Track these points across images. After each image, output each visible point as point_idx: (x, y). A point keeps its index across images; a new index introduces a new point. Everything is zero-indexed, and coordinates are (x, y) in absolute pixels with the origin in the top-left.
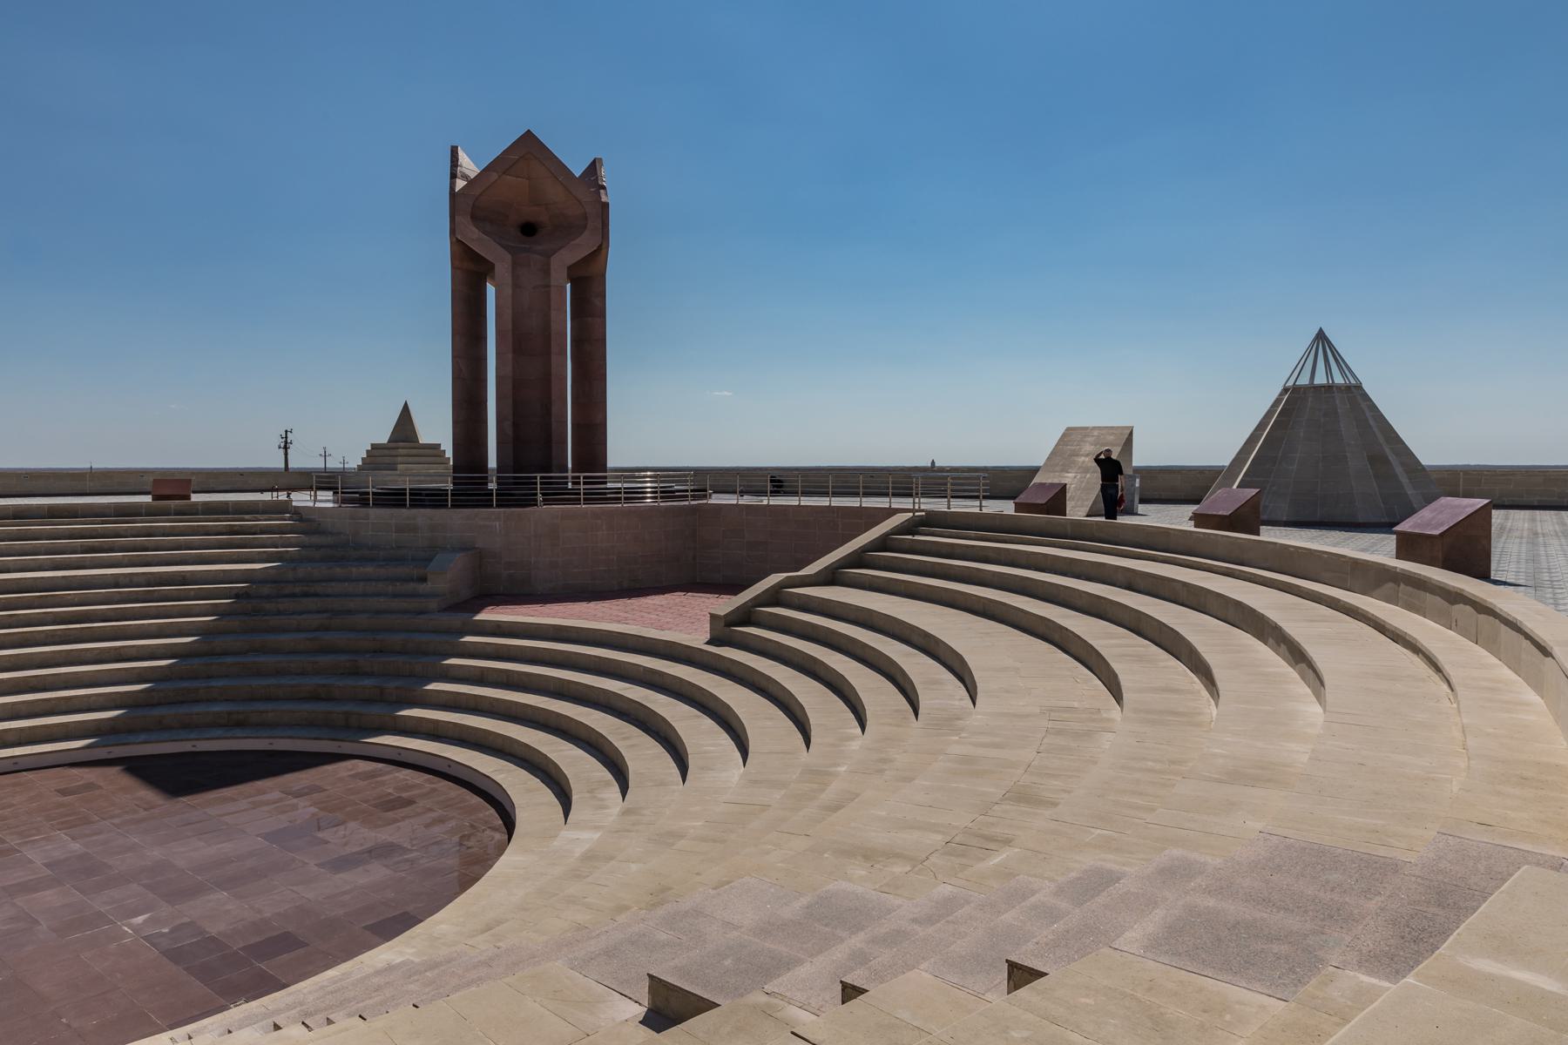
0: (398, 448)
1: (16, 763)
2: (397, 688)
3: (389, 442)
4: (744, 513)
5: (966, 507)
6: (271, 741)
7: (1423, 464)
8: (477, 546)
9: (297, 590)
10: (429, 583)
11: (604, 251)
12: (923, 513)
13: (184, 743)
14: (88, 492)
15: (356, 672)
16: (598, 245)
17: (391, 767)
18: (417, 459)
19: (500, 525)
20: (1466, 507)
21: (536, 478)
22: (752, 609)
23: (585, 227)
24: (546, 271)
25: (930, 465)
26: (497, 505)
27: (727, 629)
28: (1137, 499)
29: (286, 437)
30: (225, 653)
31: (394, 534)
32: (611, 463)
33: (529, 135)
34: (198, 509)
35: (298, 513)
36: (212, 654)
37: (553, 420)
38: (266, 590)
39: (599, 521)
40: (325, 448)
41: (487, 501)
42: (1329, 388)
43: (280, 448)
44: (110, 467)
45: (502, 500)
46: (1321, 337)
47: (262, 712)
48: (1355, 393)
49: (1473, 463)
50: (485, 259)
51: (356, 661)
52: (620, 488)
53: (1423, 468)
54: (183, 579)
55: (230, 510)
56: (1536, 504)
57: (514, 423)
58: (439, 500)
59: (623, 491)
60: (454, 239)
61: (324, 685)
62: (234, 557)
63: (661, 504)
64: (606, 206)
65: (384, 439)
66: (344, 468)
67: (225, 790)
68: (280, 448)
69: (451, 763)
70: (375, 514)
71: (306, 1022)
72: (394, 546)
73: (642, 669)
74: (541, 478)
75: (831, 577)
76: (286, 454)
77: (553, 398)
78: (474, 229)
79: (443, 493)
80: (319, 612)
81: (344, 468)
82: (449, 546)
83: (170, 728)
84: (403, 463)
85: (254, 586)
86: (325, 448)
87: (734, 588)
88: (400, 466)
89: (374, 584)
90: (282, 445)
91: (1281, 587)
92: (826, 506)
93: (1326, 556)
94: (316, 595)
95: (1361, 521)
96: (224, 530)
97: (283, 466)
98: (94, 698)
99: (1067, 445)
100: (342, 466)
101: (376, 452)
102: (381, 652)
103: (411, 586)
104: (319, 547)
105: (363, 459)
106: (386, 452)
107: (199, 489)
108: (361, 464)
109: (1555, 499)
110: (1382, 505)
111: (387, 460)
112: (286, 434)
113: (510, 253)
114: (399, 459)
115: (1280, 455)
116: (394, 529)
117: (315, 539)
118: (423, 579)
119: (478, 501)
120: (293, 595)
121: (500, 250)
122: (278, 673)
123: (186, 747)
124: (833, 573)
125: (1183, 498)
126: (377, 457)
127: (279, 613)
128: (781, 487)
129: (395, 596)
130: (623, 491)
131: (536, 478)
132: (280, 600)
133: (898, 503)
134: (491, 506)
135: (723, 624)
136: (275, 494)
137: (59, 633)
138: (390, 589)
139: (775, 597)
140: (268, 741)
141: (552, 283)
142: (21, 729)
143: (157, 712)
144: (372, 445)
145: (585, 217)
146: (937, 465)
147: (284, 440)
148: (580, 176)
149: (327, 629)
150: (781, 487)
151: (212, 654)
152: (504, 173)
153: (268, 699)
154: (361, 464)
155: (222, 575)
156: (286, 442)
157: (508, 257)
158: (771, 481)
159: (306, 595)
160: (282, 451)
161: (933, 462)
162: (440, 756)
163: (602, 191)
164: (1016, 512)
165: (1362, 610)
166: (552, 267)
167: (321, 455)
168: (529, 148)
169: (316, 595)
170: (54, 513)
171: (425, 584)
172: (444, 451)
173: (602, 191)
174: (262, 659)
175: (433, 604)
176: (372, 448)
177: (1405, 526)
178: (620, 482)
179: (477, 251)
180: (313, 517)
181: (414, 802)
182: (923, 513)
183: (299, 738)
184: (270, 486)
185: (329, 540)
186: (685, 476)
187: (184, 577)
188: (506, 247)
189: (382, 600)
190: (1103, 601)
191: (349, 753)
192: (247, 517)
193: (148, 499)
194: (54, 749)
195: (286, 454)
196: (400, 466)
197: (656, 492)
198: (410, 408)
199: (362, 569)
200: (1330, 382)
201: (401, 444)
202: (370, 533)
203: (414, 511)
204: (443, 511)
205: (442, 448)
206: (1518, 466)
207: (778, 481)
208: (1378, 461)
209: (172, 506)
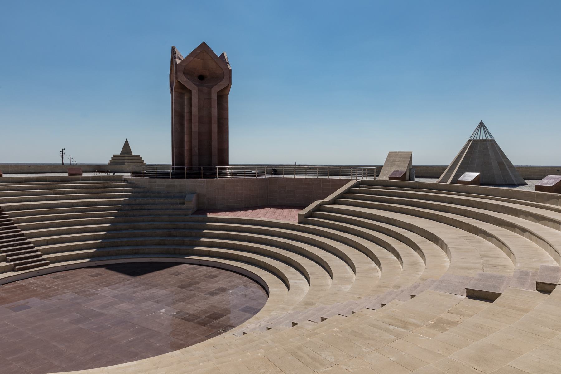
5: (372, 179)
7: (514, 165)
11: (229, 86)
12: (360, 181)
14: (9, 172)
17: (199, 266)
20: (558, 178)
21: (201, 168)
22: (313, 212)
23: (224, 77)
24: (209, 94)
25: (294, 164)
26: (203, 178)
27: (305, 219)
28: (414, 177)
29: (63, 152)
30: (121, 230)
34: (90, 179)
35: (126, 180)
36: (115, 230)
38: (127, 208)
40: (70, 156)
42: (485, 140)
43: (60, 155)
44: (27, 163)
45: (205, 176)
48: (492, 141)
49: (422, 165)
50: (186, 87)
51: (170, 232)
52: (244, 172)
53: (514, 167)
54: (96, 204)
55: (101, 179)
56: (536, 178)
60: (177, 81)
61: (162, 240)
62: (109, 196)
64: (230, 70)
65: (119, 153)
67: (149, 274)
68: (60, 155)
69: (221, 264)
70: (159, 181)
71: (234, 334)
74: (203, 168)
75: (334, 202)
76: (63, 158)
77: (212, 139)
79: (168, 173)
85: (123, 206)
86: (70, 156)
87: (302, 207)
88: (126, 163)
90: (61, 155)
91: (510, 202)
92: (316, 178)
93: (525, 192)
95: (497, 183)
97: (62, 163)
98: (83, 245)
99: (391, 158)
100: (73, 163)
101: (116, 158)
102: (176, 228)
105: (110, 160)
106: (120, 158)
107: (51, 172)
108: (109, 162)
110: (503, 179)
111: (120, 161)
112: (62, 150)
114: (126, 161)
115: (470, 162)
116: (166, 186)
117: (136, 190)
118: (184, 204)
120: (137, 209)
121: (193, 85)
123: (121, 261)
124: (335, 200)
125: (421, 176)
128: (276, 171)
129: (174, 209)
133: (353, 178)
134: (201, 178)
135: (304, 217)
136: (96, 173)
137: (61, 223)
138: (172, 207)
139: (319, 208)
140: (150, 259)
141: (212, 98)
142: (64, 256)
143: (107, 250)
145: (223, 74)
146: (297, 164)
147: (62, 152)
149: (153, 221)
150: (276, 171)
151: (115, 230)
154: (109, 162)
155: (109, 202)
156: (62, 154)
157: (197, 88)
158: (273, 169)
159: (141, 209)
160: (61, 157)
161: (295, 163)
162: (217, 262)
165: (523, 210)
167: (68, 159)
168: (203, 48)
169: (145, 209)
170: (38, 180)
172: (141, 158)
175: (190, 212)
180: (133, 182)
181: (218, 276)
182: (360, 181)
187: (96, 203)
188: (196, 85)
190: (447, 207)
192: (108, 182)
193: (66, 175)
194: (66, 264)
195: (63, 158)
196: (126, 163)
197: (231, 174)
200: (487, 138)
201: (126, 155)
202: (157, 187)
207: (275, 169)
208: (501, 164)
209: (80, 178)
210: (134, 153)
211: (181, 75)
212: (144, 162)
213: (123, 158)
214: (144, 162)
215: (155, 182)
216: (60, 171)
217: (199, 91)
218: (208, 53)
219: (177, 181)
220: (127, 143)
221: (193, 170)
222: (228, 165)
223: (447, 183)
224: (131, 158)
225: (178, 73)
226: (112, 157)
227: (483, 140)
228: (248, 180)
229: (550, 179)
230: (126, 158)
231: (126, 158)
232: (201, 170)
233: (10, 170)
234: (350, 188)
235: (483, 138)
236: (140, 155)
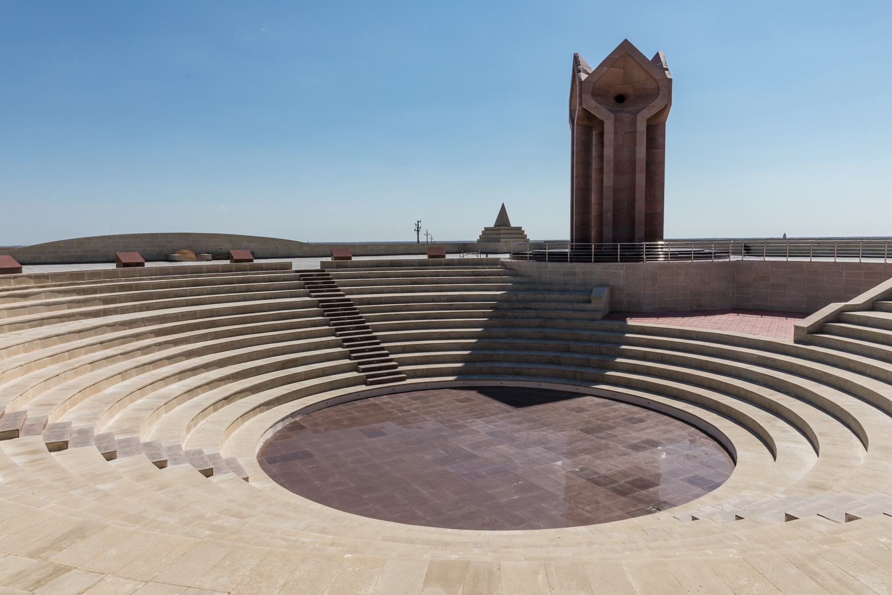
1: (614, 395)
2: (598, 360)
3: (495, 226)
4: (770, 266)
6: (577, 387)
8: (610, 284)
9: (521, 306)
10: (592, 304)
11: (667, 109)
13: (567, 386)
15: (568, 350)
16: (665, 105)
17: (612, 402)
18: (510, 236)
19: (623, 272)
21: (617, 245)
23: (658, 94)
25: (782, 237)
26: (620, 261)
27: (809, 336)
30: (496, 337)
31: (562, 277)
34: (455, 263)
37: (636, 211)
39: (680, 271)
40: (427, 231)
41: (543, 258)
43: (415, 230)
45: (598, 258)
47: (529, 368)
55: (470, 263)
57: (613, 214)
58: (587, 258)
59: (693, 252)
61: (556, 357)
63: (671, 262)
65: (492, 224)
66: (427, 242)
72: (562, 283)
73: (756, 356)
74: (620, 245)
76: (418, 234)
78: (593, 101)
79: (565, 254)
80: (535, 318)
81: (427, 242)
82: (594, 284)
83: (485, 374)
84: (504, 238)
86: (427, 231)
88: (502, 240)
89: (561, 304)
94: (530, 309)
96: (471, 274)
97: (417, 241)
98: (447, 356)
101: (487, 232)
102: (577, 340)
103: (582, 306)
104: (522, 284)
105: (480, 236)
106: (494, 232)
108: (479, 238)
109: (53, 259)
111: (494, 236)
113: (613, 114)
114: (502, 236)
116: (562, 273)
117: (518, 279)
118: (589, 302)
119: (609, 258)
122: (527, 348)
124: (873, 303)
126: (488, 235)
127: (515, 318)
130: (693, 252)
131: (643, 245)
132: (515, 311)
134: (617, 261)
135: (806, 332)
136: (462, 255)
139: (838, 317)
140: (537, 383)
141: (637, 130)
143: (478, 365)
144: (485, 228)
145: (658, 88)
146: (788, 237)
148: (651, 60)
149: (543, 327)
152: (611, 67)
153: (527, 362)
154: (479, 238)
156: (418, 228)
157: (612, 116)
159: (525, 309)
160: (416, 232)
161: (785, 235)
163: (666, 72)
164: (117, 267)
166: (637, 120)
168: (626, 51)
169: (530, 309)
170: (393, 264)
171: (590, 305)
173: (666, 72)
174: (518, 341)
175: (599, 316)
178: (668, 248)
179: (592, 113)
181: (644, 421)
183: (555, 383)
185: (526, 279)
186: (833, 243)
188: (611, 111)
189: (569, 312)
191: (583, 392)
192: (479, 267)
193: (425, 257)
195: (418, 234)
196: (502, 240)
197: (668, 254)
199: (551, 296)
201: (502, 227)
202: (548, 276)
203: (574, 264)
204: (590, 264)
207: (748, 247)
215: (546, 267)
218: (632, 57)
226: (482, 231)
230: (502, 231)
232: (617, 249)
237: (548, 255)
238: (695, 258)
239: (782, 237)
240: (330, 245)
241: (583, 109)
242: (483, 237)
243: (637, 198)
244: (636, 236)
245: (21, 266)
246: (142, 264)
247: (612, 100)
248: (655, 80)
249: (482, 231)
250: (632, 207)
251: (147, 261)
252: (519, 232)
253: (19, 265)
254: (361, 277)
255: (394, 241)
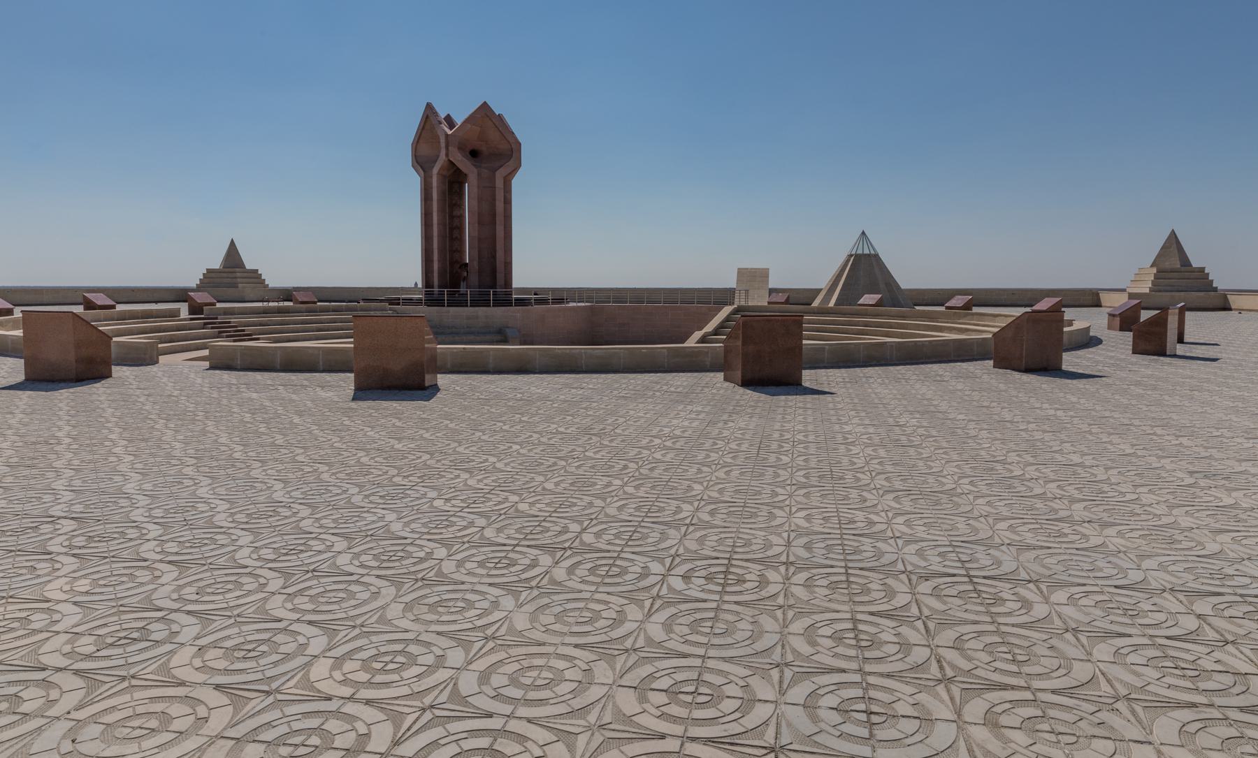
0: (235, 273)
21: (490, 291)
25: (413, 286)
32: (514, 286)
33: (485, 103)
42: (869, 255)
46: (863, 233)
48: (876, 256)
65: (216, 264)
74: (470, 291)
78: (459, 154)
101: (213, 275)
105: (200, 279)
106: (225, 275)
108: (199, 283)
114: (239, 280)
144: (207, 269)
154: (199, 283)
157: (475, 170)
176: (207, 272)
177: (946, 305)
184: (261, 299)
196: (240, 285)
198: (236, 243)
201: (237, 270)
205: (259, 273)
206: (45, 287)
210: (248, 267)
211: (453, 150)
212: (1214, 286)
213: (233, 275)
214: (1214, 286)
215: (449, 312)
216: (124, 300)
217: (479, 174)
218: (490, 119)
219: (481, 311)
220: (232, 242)
221: (499, 295)
222: (512, 288)
223: (685, 345)
224: (245, 275)
225: (450, 148)
226: (204, 274)
227: (866, 255)
228: (631, 306)
229: (958, 299)
230: (238, 275)
231: (238, 275)
232: (490, 295)
233: (45, 299)
234: (723, 322)
235: (865, 253)
236: (257, 270)
237: (515, 300)
238: (553, 303)
239: (413, 286)
240: (11, 290)
241: (449, 160)
242: (206, 280)
243: (497, 248)
244: (498, 284)
245: (13, 307)
246: (214, 304)
247: (468, 153)
248: (509, 142)
249: (204, 274)
250: (494, 257)
251: (218, 302)
252: (255, 276)
253: (114, 303)
254: (260, 325)
255: (135, 285)
